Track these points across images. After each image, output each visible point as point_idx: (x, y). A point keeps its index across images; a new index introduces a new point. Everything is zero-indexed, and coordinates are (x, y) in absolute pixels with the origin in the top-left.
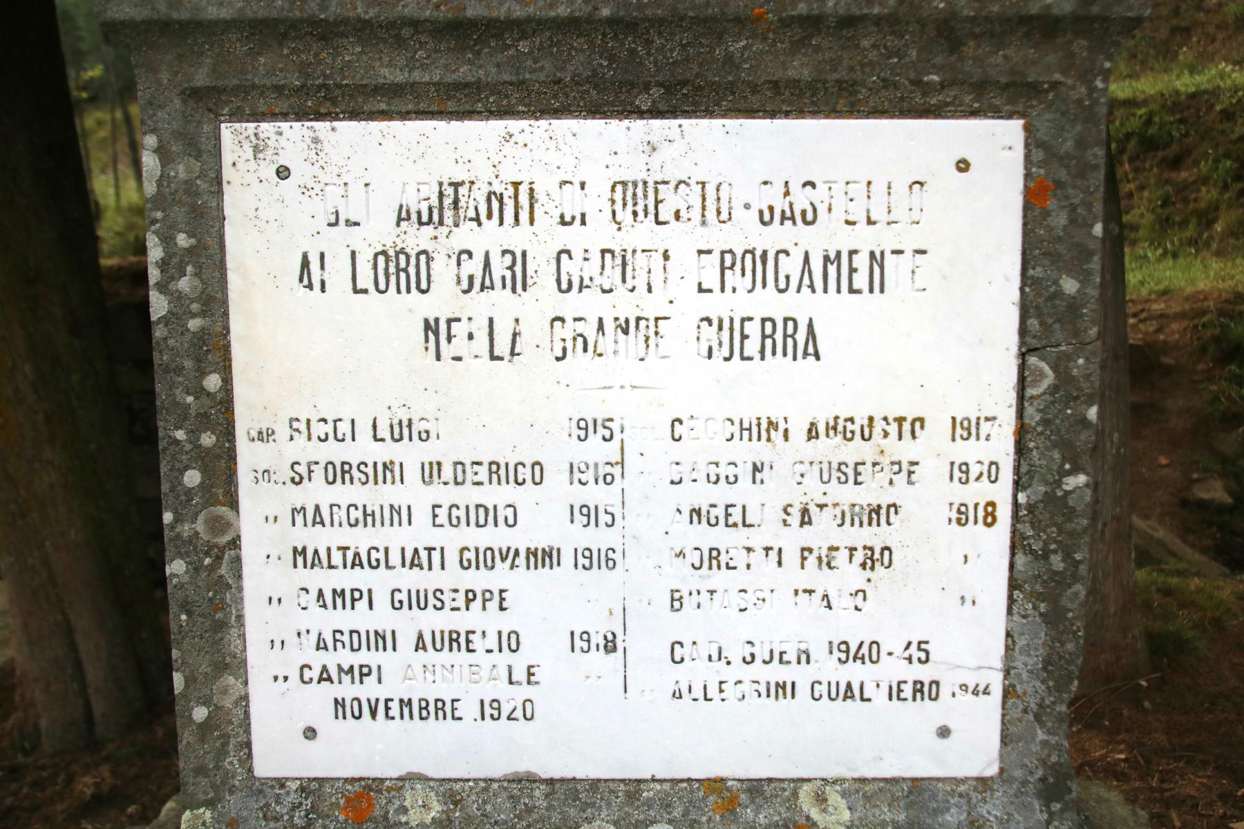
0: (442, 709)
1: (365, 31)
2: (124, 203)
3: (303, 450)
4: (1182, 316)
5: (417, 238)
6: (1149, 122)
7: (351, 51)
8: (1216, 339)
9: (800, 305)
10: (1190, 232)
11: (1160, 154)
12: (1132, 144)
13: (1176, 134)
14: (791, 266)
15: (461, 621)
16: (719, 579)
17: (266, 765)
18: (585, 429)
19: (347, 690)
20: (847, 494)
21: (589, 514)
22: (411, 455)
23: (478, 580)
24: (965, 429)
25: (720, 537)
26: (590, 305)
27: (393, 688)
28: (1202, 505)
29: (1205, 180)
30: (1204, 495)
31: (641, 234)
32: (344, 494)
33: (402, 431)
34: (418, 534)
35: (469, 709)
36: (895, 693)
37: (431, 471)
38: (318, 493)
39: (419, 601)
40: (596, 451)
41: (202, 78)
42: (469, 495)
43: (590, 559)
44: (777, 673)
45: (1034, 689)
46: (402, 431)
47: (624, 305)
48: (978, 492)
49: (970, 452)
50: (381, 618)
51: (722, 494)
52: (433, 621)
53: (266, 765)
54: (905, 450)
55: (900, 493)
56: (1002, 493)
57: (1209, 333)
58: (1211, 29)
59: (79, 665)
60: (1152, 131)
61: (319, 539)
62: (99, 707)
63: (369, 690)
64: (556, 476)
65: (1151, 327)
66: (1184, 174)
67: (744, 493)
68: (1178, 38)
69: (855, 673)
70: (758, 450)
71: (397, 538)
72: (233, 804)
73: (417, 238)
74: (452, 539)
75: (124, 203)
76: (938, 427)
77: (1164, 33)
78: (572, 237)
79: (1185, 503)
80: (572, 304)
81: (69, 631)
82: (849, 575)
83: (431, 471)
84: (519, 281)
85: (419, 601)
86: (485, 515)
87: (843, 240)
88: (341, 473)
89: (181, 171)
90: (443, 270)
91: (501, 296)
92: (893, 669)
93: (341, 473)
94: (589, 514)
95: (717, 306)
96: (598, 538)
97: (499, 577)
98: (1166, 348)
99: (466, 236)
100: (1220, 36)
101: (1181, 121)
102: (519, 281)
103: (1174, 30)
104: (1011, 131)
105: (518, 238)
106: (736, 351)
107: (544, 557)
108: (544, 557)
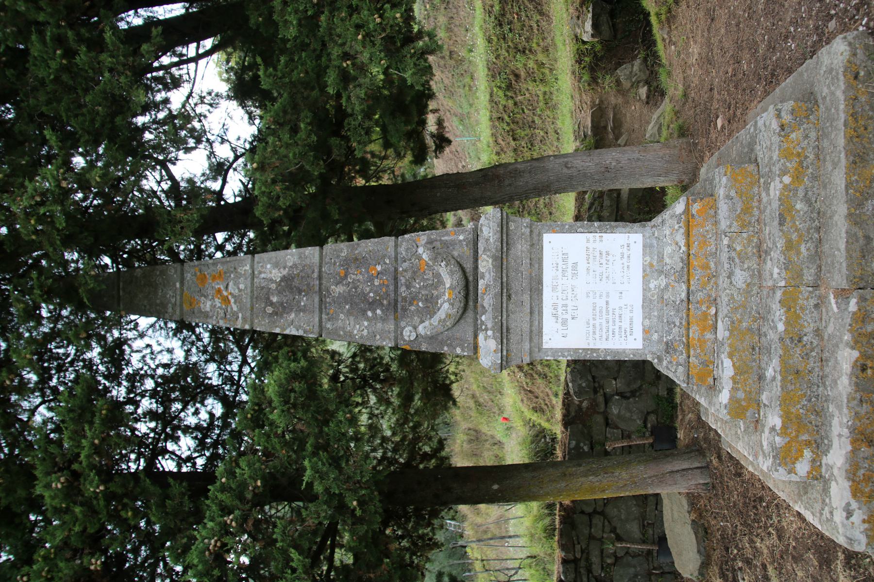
0: (631, 319)
1: (531, 326)
2: (528, 544)
3: (591, 338)
4: (580, 94)
5: (560, 320)
6: (500, 87)
7: (534, 328)
8: (589, 85)
9: (570, 265)
10: (547, 71)
11: (513, 82)
12: (509, 94)
13: (505, 76)
14: (564, 267)
15: (617, 316)
16: (611, 277)
17: (641, 347)
18: (588, 296)
19: (628, 333)
20: (598, 258)
21: (601, 296)
22: (592, 322)
23: (611, 313)
24: (588, 241)
25: (604, 276)
26: (570, 295)
27: (628, 326)
28: (648, 97)
29: (525, 65)
30: (645, 96)
31: (560, 288)
32: (597, 333)
33: (588, 323)
34: (604, 321)
35: (631, 315)
36: (629, 250)
37: (594, 319)
38: (597, 336)
39: (614, 322)
40: (591, 295)
41: (537, 350)
42: (598, 314)
43: (608, 296)
44: (626, 268)
45: (628, 229)
46: (588, 323)
47: (570, 290)
48: (598, 238)
49: (591, 240)
50: (617, 327)
51: (598, 276)
52: (617, 320)
53: (641, 347)
54: (591, 249)
55: (598, 250)
56: (598, 235)
57: (587, 88)
58: (451, 42)
59: (683, 470)
60: (503, 85)
61: (604, 337)
62: (697, 465)
63: (628, 330)
64: (595, 301)
65: (585, 106)
66: (522, 73)
67: (597, 273)
68: (455, 56)
69: (625, 256)
70: (591, 271)
71: (604, 324)
72: (646, 352)
73: (560, 320)
74: (605, 317)
75: (528, 544)
76: (588, 245)
77: (453, 62)
78: (560, 298)
79: (647, 103)
80: (569, 298)
81: (672, 472)
82: (610, 257)
83: (594, 319)
84: (566, 306)
85: (614, 322)
86: (601, 311)
87: (560, 259)
88: (594, 333)
89: (550, 353)
90: (565, 316)
91: (568, 308)
92: (625, 250)
93: (594, 333)
94: (601, 296)
95: (570, 277)
96: (604, 295)
97: (610, 309)
98: (593, 102)
99: (559, 313)
100: (454, 38)
101: (499, 74)
102: (566, 306)
103: (451, 58)
104: (545, 235)
105: (560, 306)
106: (577, 274)
107: (607, 303)
108: (607, 303)
